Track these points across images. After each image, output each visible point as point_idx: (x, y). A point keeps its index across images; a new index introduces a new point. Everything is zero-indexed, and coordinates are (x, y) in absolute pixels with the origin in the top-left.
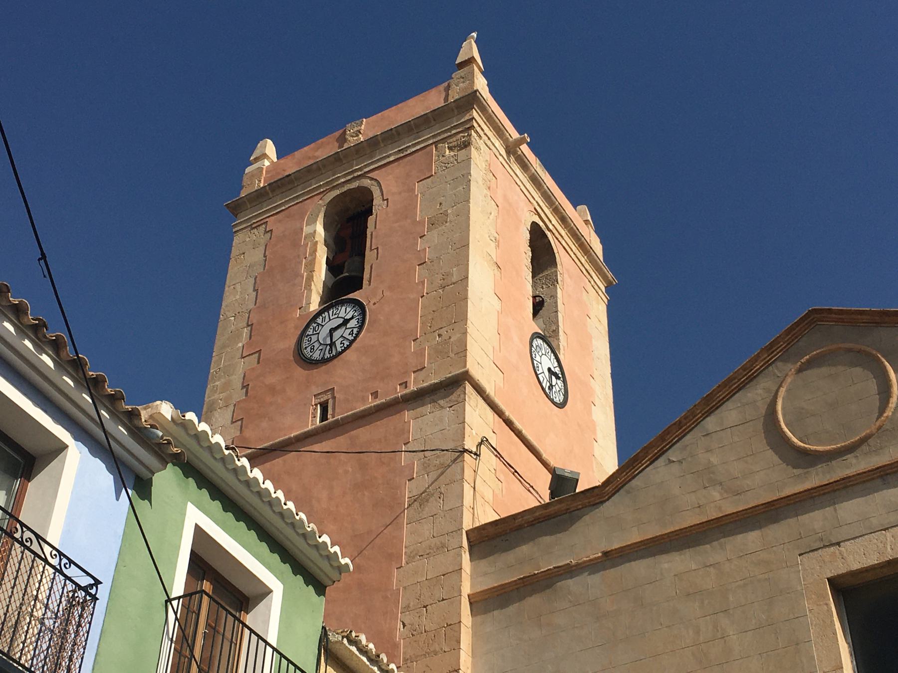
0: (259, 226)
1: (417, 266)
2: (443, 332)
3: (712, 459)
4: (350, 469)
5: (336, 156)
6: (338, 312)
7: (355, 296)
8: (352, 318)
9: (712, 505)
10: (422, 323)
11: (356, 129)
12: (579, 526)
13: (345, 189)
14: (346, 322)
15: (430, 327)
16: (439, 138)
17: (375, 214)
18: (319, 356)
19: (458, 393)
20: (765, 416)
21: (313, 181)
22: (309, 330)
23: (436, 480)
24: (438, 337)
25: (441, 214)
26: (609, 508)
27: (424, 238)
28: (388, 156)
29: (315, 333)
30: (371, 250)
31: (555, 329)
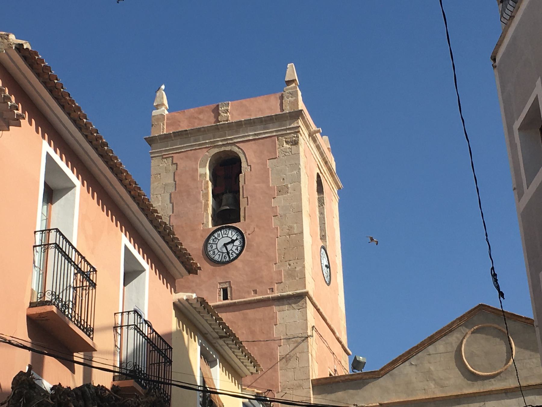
0: (168, 157)
1: (273, 217)
2: (291, 262)
3: (431, 367)
4: (244, 332)
5: (216, 126)
6: (227, 233)
7: (236, 225)
8: (237, 239)
9: (430, 390)
10: (279, 254)
11: (225, 108)
12: (368, 387)
13: (223, 149)
14: (233, 241)
15: (284, 258)
16: (279, 133)
17: (244, 173)
18: (219, 258)
19: (303, 302)
20: (456, 351)
21: (201, 137)
22: (210, 240)
23: (293, 350)
24: (288, 265)
25: (284, 186)
26: (383, 381)
27: (275, 199)
28: (249, 136)
29: (214, 243)
30: (243, 198)
31: (324, 234)
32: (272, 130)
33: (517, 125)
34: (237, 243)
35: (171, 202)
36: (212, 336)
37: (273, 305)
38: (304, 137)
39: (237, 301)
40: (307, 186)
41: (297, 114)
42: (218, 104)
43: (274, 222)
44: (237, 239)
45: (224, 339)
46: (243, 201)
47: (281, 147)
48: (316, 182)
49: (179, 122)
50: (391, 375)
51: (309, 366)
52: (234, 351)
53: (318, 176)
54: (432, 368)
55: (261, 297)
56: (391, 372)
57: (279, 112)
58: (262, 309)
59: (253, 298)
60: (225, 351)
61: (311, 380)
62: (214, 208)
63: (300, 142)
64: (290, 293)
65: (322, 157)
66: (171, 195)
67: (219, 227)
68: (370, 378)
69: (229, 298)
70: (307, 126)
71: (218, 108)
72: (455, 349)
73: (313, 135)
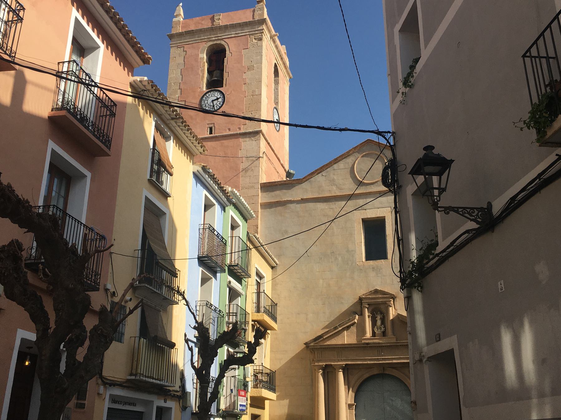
0: (181, 47)
2: (253, 112)
8: (220, 98)
9: (333, 191)
11: (218, 17)
13: (215, 42)
14: (218, 99)
21: (202, 35)
26: (305, 185)
28: (231, 34)
30: (226, 72)
32: (247, 30)
33: (398, 26)
34: (220, 100)
35: (181, 75)
36: (166, 118)
37: (240, 138)
38: (267, 37)
39: (217, 135)
40: (266, 67)
41: (263, 21)
42: (213, 15)
43: (244, 88)
44: (220, 98)
45: (175, 120)
46: (225, 75)
47: (251, 41)
48: (273, 68)
49: (189, 25)
50: (310, 182)
51: (259, 175)
52: (193, 142)
53: (276, 66)
54: (335, 178)
55: (233, 133)
56: (310, 180)
57: (251, 20)
58: (233, 140)
59: (228, 133)
60: (178, 132)
61: (260, 184)
62: (208, 80)
63: (263, 39)
64: (251, 131)
65: (279, 54)
66: (181, 70)
67: (210, 90)
68: (296, 183)
69: (213, 133)
70: (269, 31)
71: (214, 17)
72: (351, 167)
73: (273, 38)
